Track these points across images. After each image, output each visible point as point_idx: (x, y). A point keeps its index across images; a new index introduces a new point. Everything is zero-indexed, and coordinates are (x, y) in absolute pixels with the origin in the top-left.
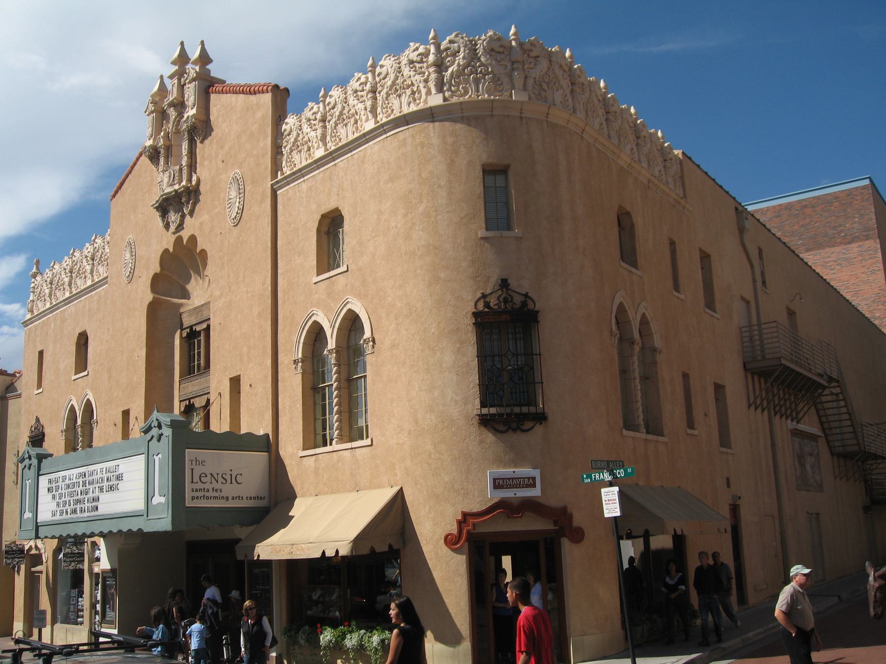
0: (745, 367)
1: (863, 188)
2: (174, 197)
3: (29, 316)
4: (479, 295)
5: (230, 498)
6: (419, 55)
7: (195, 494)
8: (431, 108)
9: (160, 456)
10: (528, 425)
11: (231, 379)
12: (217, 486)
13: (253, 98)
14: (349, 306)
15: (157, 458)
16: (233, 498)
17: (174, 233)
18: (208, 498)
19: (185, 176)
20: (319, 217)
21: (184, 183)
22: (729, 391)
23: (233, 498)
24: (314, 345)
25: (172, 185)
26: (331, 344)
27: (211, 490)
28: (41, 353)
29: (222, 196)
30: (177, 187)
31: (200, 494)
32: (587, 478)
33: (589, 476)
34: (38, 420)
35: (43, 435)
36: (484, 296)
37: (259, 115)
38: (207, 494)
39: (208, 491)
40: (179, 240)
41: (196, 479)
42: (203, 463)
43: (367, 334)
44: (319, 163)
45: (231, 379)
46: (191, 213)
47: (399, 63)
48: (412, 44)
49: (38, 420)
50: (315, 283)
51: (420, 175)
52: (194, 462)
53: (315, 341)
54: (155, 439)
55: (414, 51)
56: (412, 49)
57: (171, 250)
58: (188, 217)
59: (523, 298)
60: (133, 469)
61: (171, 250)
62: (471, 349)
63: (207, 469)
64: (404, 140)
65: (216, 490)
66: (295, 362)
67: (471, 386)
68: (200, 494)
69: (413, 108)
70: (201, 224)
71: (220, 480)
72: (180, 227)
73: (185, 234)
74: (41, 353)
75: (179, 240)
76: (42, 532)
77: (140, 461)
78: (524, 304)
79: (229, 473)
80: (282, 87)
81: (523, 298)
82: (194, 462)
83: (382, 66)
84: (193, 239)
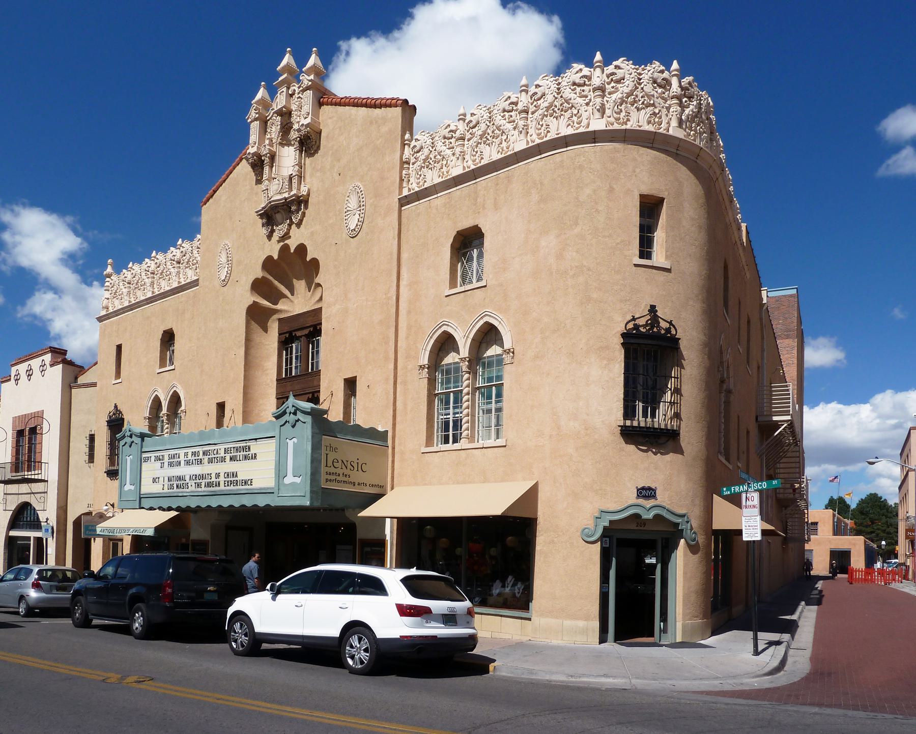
1: (791, 296)
2: (283, 205)
3: (104, 313)
4: (630, 318)
6: (582, 77)
7: (329, 477)
9: (295, 440)
10: (663, 440)
11: (345, 380)
12: (347, 472)
19: (295, 185)
20: (454, 233)
21: (294, 192)
22: (751, 434)
25: (280, 193)
26: (165, 410)
28: (119, 348)
29: (338, 207)
30: (286, 195)
31: (333, 477)
34: (116, 407)
35: (123, 420)
37: (385, 129)
38: (338, 478)
40: (285, 248)
41: (330, 463)
42: (335, 450)
43: (183, 408)
44: (458, 181)
45: (345, 380)
46: (299, 225)
47: (559, 84)
49: (116, 407)
55: (577, 72)
56: (575, 70)
57: (276, 257)
58: (294, 226)
59: (668, 325)
60: (266, 451)
62: (617, 366)
64: (562, 161)
66: (422, 367)
67: (615, 399)
68: (333, 477)
70: (312, 233)
71: (349, 466)
72: (286, 236)
73: (293, 244)
74: (119, 348)
75: (285, 248)
77: (272, 445)
78: (668, 330)
79: (356, 461)
81: (668, 325)
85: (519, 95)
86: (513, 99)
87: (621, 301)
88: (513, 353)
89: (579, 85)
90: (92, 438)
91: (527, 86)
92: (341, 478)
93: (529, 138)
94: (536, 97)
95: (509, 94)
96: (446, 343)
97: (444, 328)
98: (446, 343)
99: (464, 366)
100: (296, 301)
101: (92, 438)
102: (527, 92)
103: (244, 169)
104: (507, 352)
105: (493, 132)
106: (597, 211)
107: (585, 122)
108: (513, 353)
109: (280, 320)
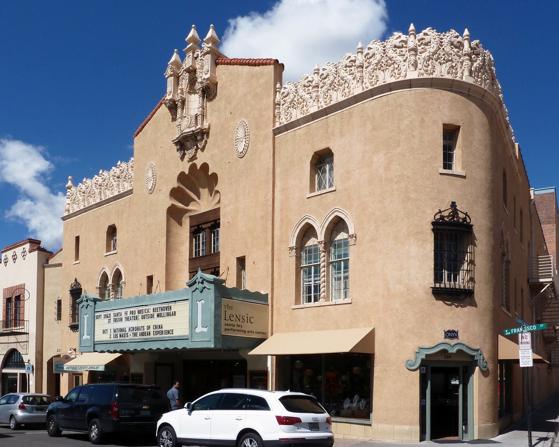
0: (528, 281)
1: (551, 194)
2: (191, 135)
3: (66, 214)
4: (437, 211)
5: (247, 332)
6: (401, 42)
8: (410, 80)
9: (203, 301)
10: (462, 297)
12: (239, 323)
13: (257, 68)
14: (104, 270)
15: (85, 317)
16: (248, 332)
17: (189, 162)
18: (234, 330)
19: (199, 121)
21: (199, 126)
23: (248, 332)
24: (302, 239)
27: (236, 326)
28: (78, 238)
29: (230, 136)
30: (194, 129)
31: (230, 327)
32: (508, 332)
33: (510, 331)
34: (76, 280)
36: (440, 212)
37: (262, 81)
38: (234, 328)
39: (234, 326)
40: (193, 167)
41: (228, 318)
43: (123, 280)
46: (203, 149)
47: (385, 47)
48: (395, 33)
49: (76, 280)
50: (441, 174)
51: (399, 127)
52: (226, 307)
53: (304, 236)
54: (84, 307)
55: (397, 38)
57: (187, 172)
58: (199, 151)
59: (464, 216)
61: (187, 172)
62: (429, 245)
63: (234, 312)
64: (388, 101)
65: (239, 326)
67: (428, 269)
68: (230, 327)
69: (393, 80)
70: (212, 155)
71: (241, 319)
72: (194, 158)
73: (199, 163)
74: (78, 238)
75: (193, 167)
76: (98, 348)
78: (464, 220)
80: (280, 63)
82: (226, 307)
83: (369, 49)
84: (205, 166)
85: (356, 55)
86: (353, 58)
87: (431, 199)
88: (356, 237)
89: (399, 47)
90: (59, 303)
91: (362, 48)
92: (236, 328)
93: (364, 86)
94: (368, 56)
95: (350, 54)
96: (308, 231)
97: (336, 214)
98: (308, 231)
99: (321, 247)
100: (201, 203)
101: (59, 303)
102: (362, 53)
103: (163, 111)
104: (351, 236)
105: (339, 81)
106: (413, 136)
107: (403, 74)
108: (356, 237)
109: (190, 217)
